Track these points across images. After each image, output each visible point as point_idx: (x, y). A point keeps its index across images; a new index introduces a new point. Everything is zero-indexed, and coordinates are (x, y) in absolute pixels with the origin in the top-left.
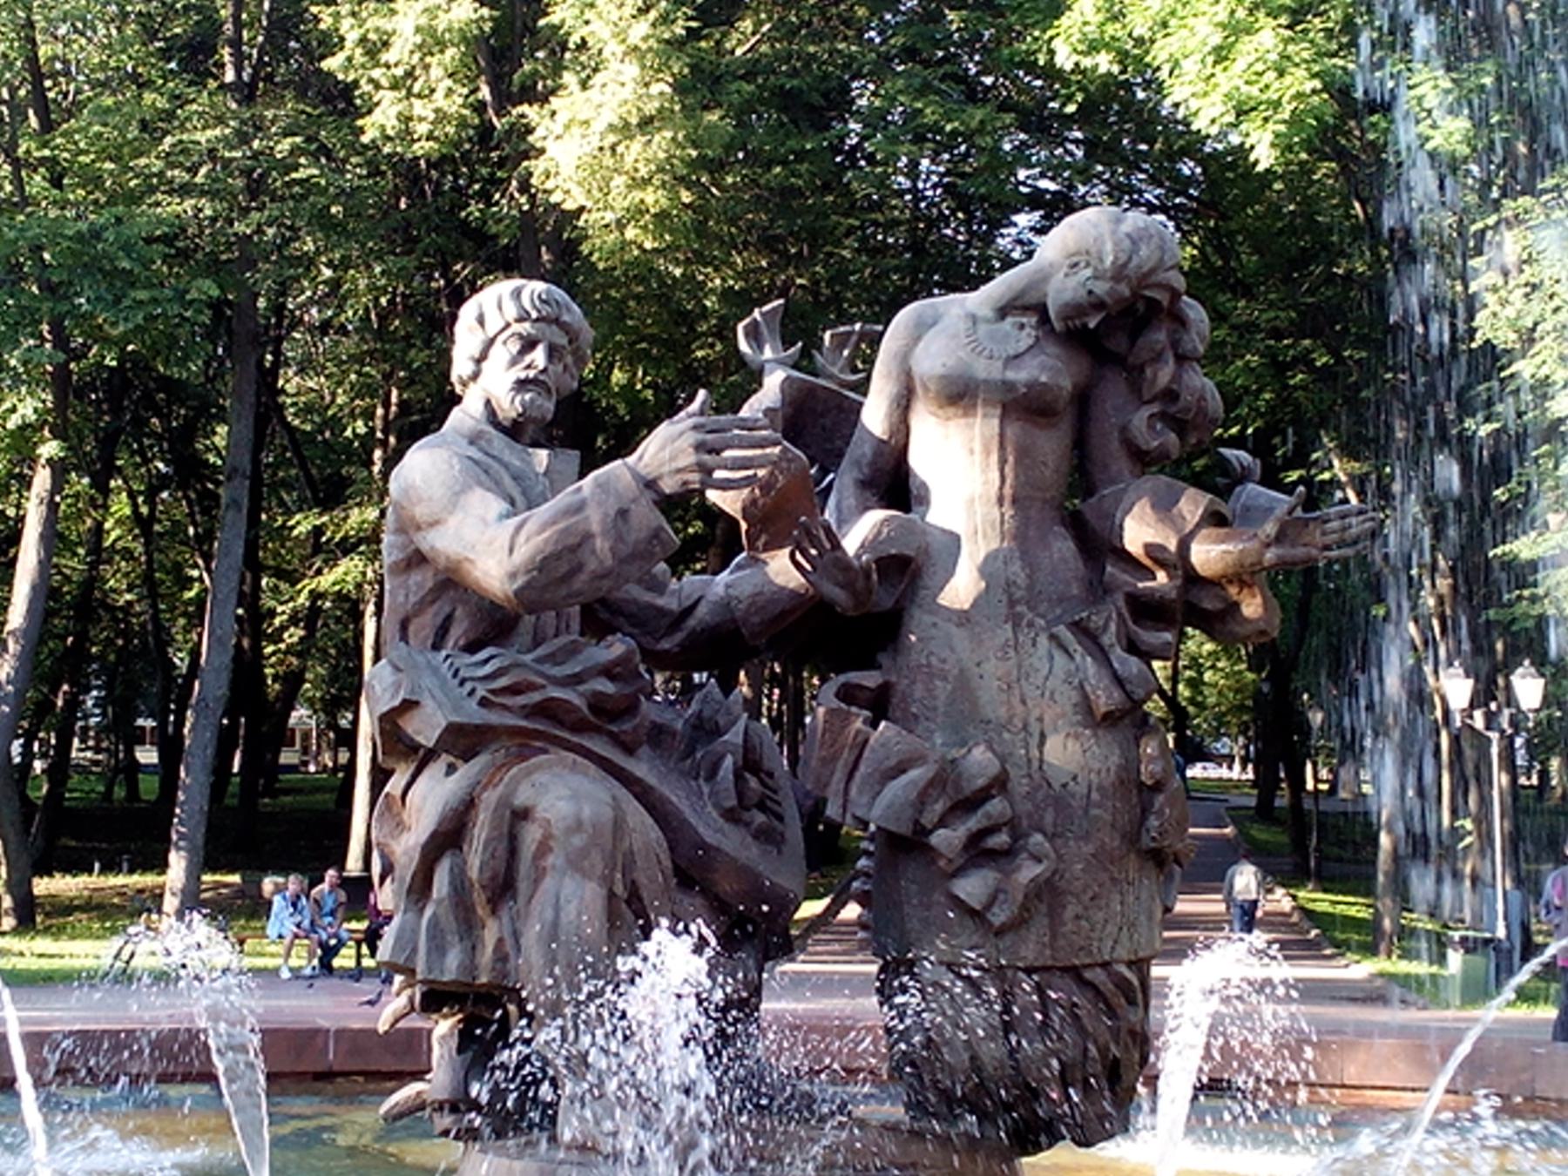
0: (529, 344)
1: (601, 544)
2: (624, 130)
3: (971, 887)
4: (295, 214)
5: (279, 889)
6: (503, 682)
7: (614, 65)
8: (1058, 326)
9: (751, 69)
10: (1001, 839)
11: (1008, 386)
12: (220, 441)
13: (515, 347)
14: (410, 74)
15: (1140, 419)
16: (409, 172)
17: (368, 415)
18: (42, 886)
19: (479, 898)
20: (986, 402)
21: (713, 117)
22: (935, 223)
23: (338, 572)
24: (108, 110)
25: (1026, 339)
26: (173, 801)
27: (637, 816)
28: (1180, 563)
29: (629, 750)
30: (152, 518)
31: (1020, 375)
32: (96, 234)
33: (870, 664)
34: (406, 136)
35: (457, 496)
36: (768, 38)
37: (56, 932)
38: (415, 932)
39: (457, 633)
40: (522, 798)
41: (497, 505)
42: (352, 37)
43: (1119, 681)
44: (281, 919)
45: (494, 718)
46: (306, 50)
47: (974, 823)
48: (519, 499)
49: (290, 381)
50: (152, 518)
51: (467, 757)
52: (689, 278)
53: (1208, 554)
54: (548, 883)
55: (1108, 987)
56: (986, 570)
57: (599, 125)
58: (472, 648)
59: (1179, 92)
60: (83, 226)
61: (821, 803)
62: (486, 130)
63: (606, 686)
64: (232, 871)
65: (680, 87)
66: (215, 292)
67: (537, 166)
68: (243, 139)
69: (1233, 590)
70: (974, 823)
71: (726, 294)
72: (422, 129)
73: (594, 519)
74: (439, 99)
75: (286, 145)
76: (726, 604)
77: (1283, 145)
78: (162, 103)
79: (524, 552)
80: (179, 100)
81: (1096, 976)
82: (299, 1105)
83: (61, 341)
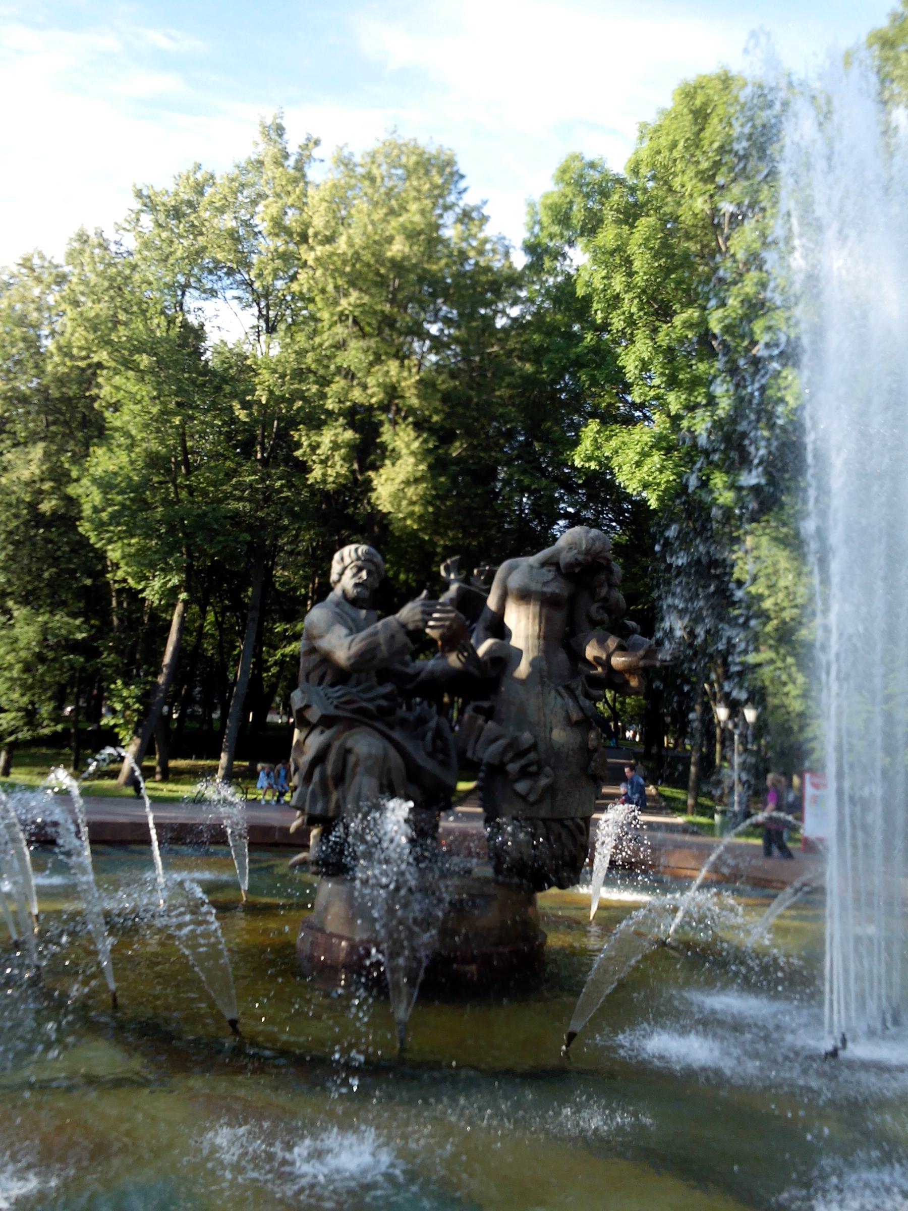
0: (360, 569)
1: (384, 648)
2: (407, 483)
3: (521, 787)
4: (282, 509)
5: (263, 769)
6: (344, 699)
7: (405, 458)
8: (563, 571)
9: (459, 460)
10: (533, 768)
11: (543, 594)
12: (249, 593)
13: (355, 570)
14: (327, 458)
15: (594, 608)
16: (326, 494)
17: (306, 587)
18: (172, 763)
19: (330, 783)
20: (535, 600)
21: (442, 479)
22: (527, 522)
23: (293, 646)
24: (212, 468)
25: (551, 576)
26: (224, 733)
27: (394, 754)
28: (607, 664)
29: (392, 728)
30: (223, 622)
31: (548, 589)
32: (205, 514)
33: (487, 698)
34: (324, 481)
35: (329, 627)
36: (465, 449)
37: (176, 782)
38: (305, 794)
39: (328, 679)
40: (349, 744)
41: (343, 631)
42: (305, 443)
43: (581, 709)
44: (263, 781)
45: (340, 713)
46: (289, 447)
47: (523, 762)
48: (354, 630)
49: (278, 572)
50: (223, 622)
51: (329, 727)
52: (430, 540)
53: (618, 661)
54: (357, 779)
55: (573, 827)
56: (533, 664)
57: (398, 481)
58: (332, 685)
59: (621, 479)
60: (200, 511)
61: (465, 751)
62: (356, 479)
63: (383, 703)
64: (245, 760)
65: (430, 467)
66: (249, 538)
67: (374, 495)
68: (262, 480)
69: (627, 676)
70: (523, 762)
71: (445, 547)
72: (331, 479)
73: (382, 638)
74: (338, 468)
75: (278, 484)
76: (431, 673)
77: (660, 499)
78: (232, 465)
79: (354, 649)
80: (240, 465)
81: (569, 823)
82: (264, 856)
83: (190, 554)
